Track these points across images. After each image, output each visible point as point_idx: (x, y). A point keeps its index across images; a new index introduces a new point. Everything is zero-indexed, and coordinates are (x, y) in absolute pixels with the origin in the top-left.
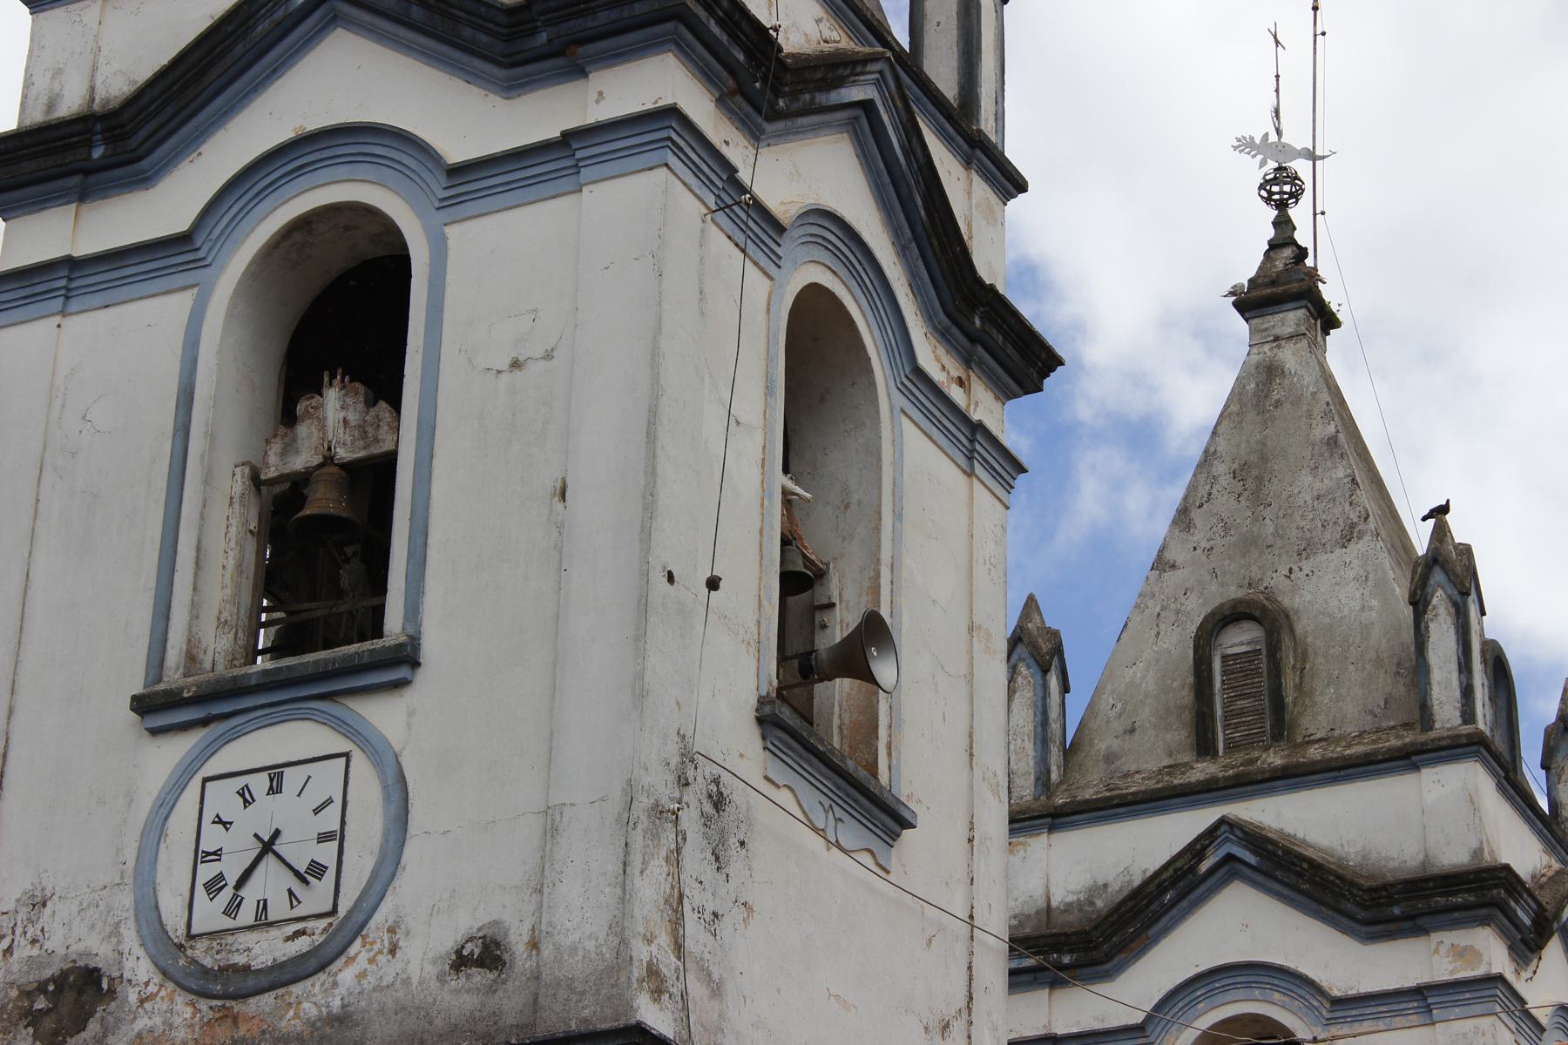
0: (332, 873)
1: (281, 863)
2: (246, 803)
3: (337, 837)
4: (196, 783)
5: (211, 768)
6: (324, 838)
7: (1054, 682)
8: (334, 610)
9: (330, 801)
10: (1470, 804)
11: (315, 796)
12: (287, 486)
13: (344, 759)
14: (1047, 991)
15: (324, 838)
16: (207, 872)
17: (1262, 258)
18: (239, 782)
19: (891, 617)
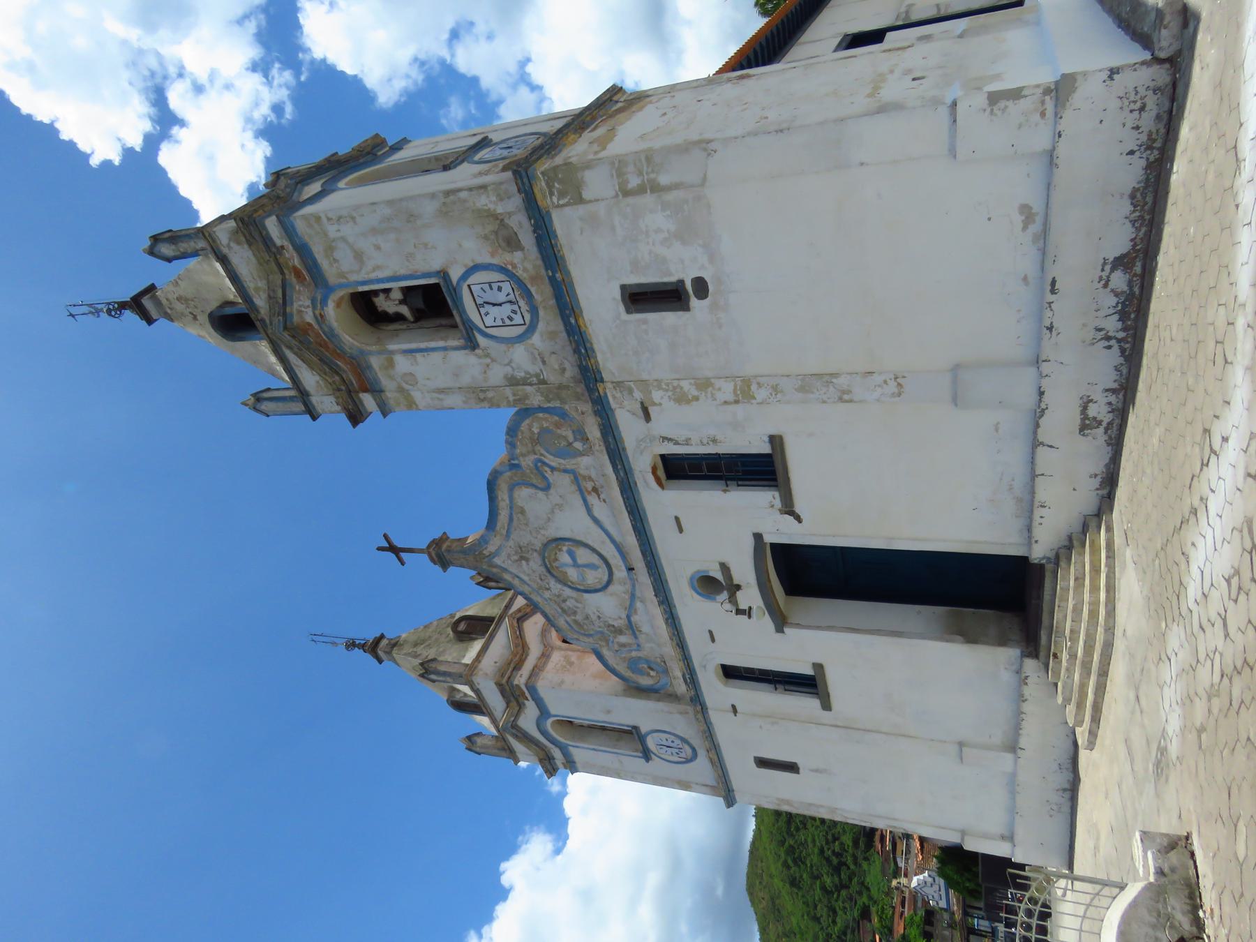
0: (499, 284)
1: (722, 758)
2: (488, 314)
3: (490, 284)
4: (488, 331)
5: (482, 327)
6: (491, 288)
7: (266, 395)
8: (889, 917)
9: (482, 288)
10: (638, 594)
11: (482, 294)
12: (951, 892)
13: (471, 286)
14: (1012, 101)
15: (491, 288)
16: (486, 287)
17: (752, 909)
18: (483, 316)
19: (1209, 480)
